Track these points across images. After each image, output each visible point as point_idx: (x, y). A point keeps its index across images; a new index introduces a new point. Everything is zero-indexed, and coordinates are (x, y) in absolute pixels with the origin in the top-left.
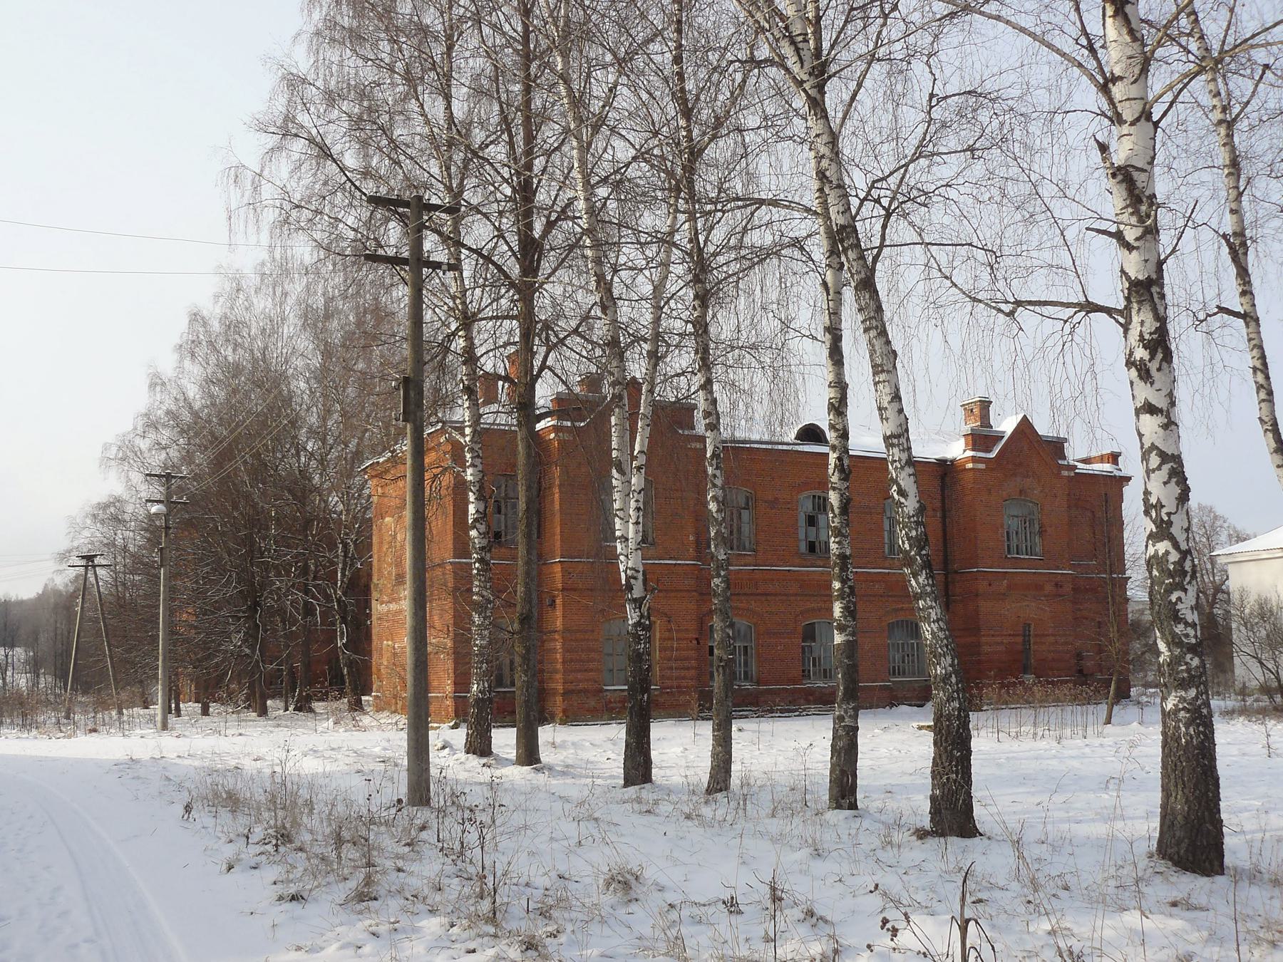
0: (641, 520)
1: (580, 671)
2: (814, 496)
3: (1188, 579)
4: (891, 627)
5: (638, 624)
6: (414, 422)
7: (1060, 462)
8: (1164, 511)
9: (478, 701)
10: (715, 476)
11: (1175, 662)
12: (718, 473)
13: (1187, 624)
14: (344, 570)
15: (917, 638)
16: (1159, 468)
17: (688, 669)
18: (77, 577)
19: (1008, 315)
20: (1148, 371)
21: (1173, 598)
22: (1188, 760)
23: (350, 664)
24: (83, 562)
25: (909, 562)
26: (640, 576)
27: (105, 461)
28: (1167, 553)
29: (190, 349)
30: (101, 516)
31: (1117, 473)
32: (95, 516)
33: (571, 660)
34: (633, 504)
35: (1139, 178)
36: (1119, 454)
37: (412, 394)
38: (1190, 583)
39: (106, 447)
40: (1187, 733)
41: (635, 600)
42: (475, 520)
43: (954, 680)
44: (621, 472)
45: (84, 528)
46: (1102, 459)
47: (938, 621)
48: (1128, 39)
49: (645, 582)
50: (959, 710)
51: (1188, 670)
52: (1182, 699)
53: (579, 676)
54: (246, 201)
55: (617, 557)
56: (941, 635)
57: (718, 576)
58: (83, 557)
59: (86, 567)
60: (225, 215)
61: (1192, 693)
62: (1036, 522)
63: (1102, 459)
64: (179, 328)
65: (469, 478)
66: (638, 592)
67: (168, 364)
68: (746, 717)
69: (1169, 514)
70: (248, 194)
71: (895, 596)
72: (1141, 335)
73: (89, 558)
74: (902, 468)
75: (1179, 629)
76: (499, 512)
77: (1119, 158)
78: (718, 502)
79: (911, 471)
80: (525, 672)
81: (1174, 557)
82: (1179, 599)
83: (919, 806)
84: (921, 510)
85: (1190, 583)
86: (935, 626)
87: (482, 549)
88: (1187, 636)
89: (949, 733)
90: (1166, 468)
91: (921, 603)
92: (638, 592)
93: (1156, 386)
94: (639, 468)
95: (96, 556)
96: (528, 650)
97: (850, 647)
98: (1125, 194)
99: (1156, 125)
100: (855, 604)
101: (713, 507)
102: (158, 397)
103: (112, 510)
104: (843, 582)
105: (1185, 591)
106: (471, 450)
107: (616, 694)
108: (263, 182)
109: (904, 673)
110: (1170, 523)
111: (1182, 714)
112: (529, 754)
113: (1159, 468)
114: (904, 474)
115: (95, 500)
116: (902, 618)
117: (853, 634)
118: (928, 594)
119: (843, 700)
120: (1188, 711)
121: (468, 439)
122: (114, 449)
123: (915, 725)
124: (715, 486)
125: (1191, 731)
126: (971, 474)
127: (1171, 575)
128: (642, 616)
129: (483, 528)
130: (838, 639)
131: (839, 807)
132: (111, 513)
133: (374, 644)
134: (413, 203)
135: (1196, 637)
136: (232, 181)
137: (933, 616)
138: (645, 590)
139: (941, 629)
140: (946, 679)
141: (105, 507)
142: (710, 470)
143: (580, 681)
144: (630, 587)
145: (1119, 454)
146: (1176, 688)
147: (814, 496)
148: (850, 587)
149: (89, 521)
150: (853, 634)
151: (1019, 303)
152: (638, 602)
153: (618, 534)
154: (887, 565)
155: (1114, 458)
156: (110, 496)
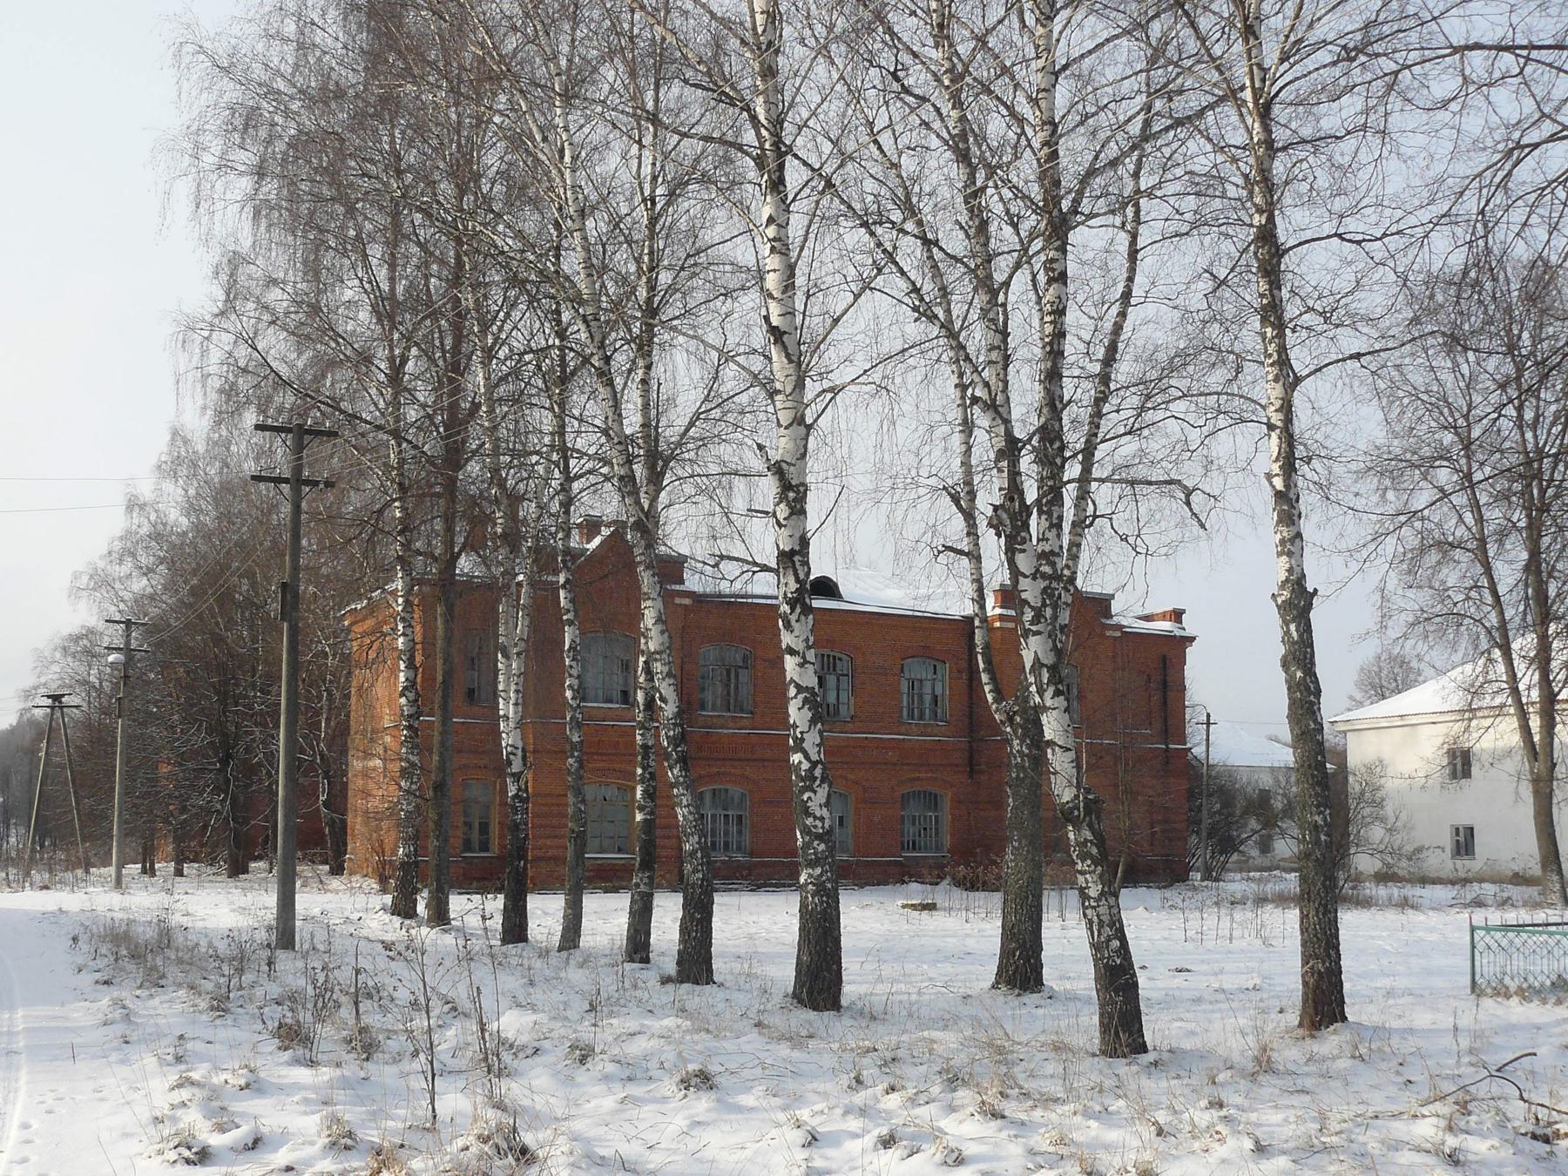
0: (520, 701)
1: (548, 837)
2: (823, 655)
3: (818, 782)
4: (905, 799)
5: (516, 796)
6: (290, 622)
7: (1103, 621)
8: (798, 730)
9: (403, 864)
10: (571, 667)
11: (807, 846)
12: (574, 664)
13: (815, 818)
14: (328, 720)
15: (936, 809)
16: (795, 697)
17: (669, 837)
18: (47, 715)
19: (713, 567)
20: (789, 622)
21: (805, 797)
22: (813, 922)
23: (332, 823)
24: (49, 702)
25: (667, 756)
26: (519, 753)
27: (75, 592)
28: (800, 762)
29: (230, 401)
30: (73, 649)
31: (1178, 633)
32: (64, 648)
33: (541, 826)
34: (513, 687)
35: (791, 472)
36: (1183, 612)
37: (289, 597)
38: (820, 786)
39: (76, 576)
40: (813, 902)
41: (513, 775)
42: (405, 688)
43: (699, 855)
44: (506, 656)
45: (52, 663)
46: (1163, 616)
47: (688, 806)
48: (785, 361)
49: (524, 758)
50: (703, 880)
51: (815, 854)
52: (810, 876)
53: (548, 842)
54: (194, 364)
55: (500, 733)
56: (691, 818)
57: (572, 756)
58: (49, 697)
59: (52, 708)
60: (173, 380)
61: (818, 871)
62: (1075, 686)
63: (1163, 616)
64: (158, 446)
65: (400, 646)
66: (516, 766)
67: (198, 425)
68: (736, 890)
69: (802, 733)
70: (196, 358)
71: (909, 764)
72: (785, 594)
73: (56, 698)
74: (663, 679)
75: (809, 821)
76: (473, 669)
77: (775, 456)
78: (573, 690)
79: (672, 681)
80: (437, 838)
81: (805, 765)
82: (809, 798)
83: (785, 973)
84: (679, 714)
85: (820, 786)
86: (685, 810)
87: (410, 716)
88: (815, 827)
89: (693, 898)
90: (800, 697)
91: (675, 791)
92: (516, 767)
93: (796, 633)
94: (518, 654)
95: (63, 695)
96: (440, 816)
97: (648, 825)
98: (777, 483)
99: (809, 427)
100: (655, 788)
101: (569, 694)
102: (136, 521)
103: (85, 642)
104: (644, 769)
105: (815, 792)
106: (403, 620)
107: (592, 862)
108: (211, 346)
109: (914, 848)
110: (802, 740)
111: (810, 887)
112: (440, 916)
113: (795, 697)
114: (664, 684)
115: (66, 631)
116: (919, 788)
117: (651, 813)
118: (682, 784)
119: (639, 869)
120: (814, 885)
121: (400, 608)
122: (85, 579)
123: (900, 903)
124: (571, 676)
125: (816, 900)
126: (999, 634)
127: (803, 780)
128: (519, 789)
129: (411, 696)
130: (639, 817)
131: (632, 960)
132: (83, 646)
133: (350, 801)
134: (295, 430)
135: (823, 827)
136: (179, 346)
137: (685, 802)
138: (525, 765)
139: (690, 813)
140: (693, 853)
141: (76, 639)
142: (567, 662)
143: (551, 847)
144: (509, 763)
145: (1183, 612)
146: (806, 867)
147: (823, 655)
148: (650, 773)
149: (58, 655)
150: (651, 813)
151: (722, 557)
152: (517, 777)
153: (501, 713)
154: (903, 729)
155: (1177, 615)
156: (83, 627)
